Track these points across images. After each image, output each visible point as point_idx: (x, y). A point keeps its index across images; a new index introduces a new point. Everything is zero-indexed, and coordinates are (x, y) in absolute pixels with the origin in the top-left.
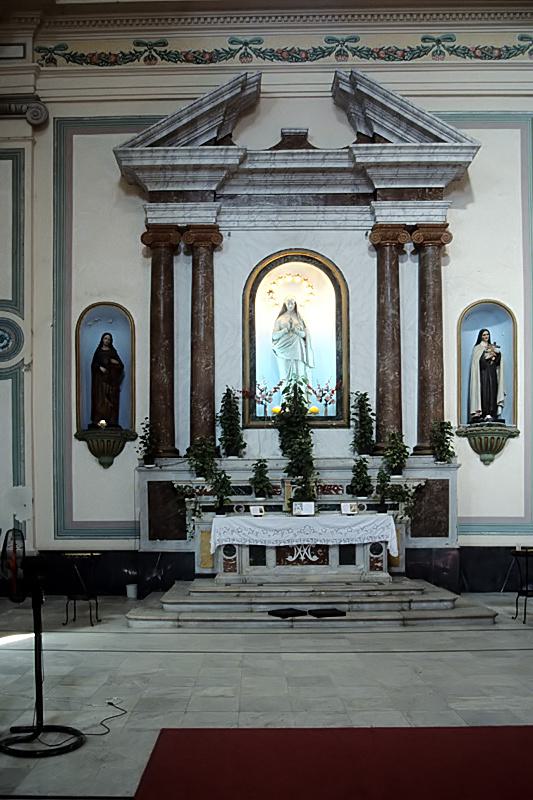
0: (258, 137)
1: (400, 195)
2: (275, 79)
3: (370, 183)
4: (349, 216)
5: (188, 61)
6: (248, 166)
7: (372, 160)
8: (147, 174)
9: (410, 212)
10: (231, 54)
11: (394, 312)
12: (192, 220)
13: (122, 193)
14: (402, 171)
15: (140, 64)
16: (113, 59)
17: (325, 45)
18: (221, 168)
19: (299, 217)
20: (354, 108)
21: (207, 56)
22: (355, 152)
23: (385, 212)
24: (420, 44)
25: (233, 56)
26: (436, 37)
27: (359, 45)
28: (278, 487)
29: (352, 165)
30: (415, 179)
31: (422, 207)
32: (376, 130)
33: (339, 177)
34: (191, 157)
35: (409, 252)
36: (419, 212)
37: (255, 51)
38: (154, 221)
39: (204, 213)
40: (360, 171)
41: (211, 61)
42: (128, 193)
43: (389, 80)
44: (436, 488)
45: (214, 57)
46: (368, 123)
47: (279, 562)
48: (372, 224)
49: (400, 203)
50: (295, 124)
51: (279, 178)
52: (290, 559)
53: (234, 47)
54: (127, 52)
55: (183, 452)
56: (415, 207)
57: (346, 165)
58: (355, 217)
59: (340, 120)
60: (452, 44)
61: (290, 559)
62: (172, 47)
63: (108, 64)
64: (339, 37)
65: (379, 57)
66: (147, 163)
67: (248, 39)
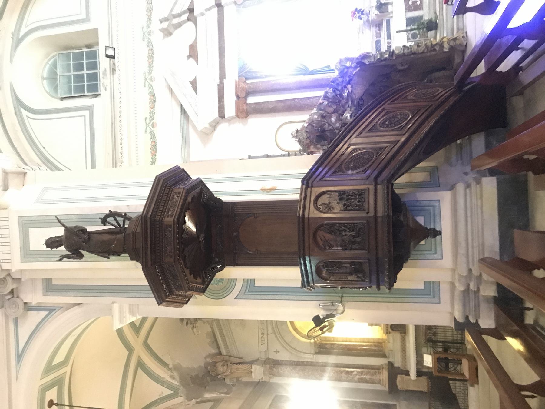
16: (153, 144)
17: (146, 42)
18: (17, 113)
37: (149, 75)
52: (419, 3)
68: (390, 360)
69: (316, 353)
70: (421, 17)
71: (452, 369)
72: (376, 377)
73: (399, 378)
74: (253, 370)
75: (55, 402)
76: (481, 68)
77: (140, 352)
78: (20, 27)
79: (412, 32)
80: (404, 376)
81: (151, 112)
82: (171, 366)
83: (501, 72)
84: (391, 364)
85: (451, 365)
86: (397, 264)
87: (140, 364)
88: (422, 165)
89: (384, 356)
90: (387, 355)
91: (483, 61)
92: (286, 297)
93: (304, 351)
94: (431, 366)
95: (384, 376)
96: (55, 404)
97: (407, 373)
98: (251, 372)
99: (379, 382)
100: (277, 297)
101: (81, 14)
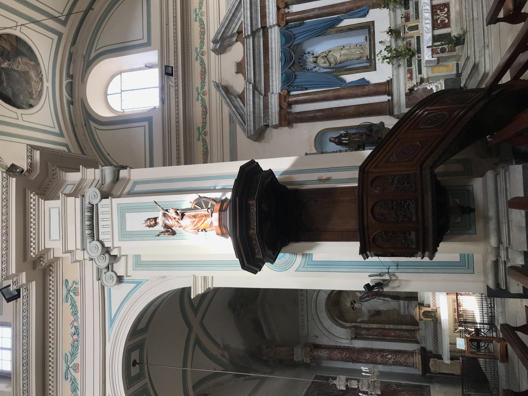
0: (239, 84)
1: (264, 16)
2: (214, 76)
3: (258, 30)
4: (273, 37)
5: (206, 118)
6: (253, 81)
7: (249, 28)
8: (257, 125)
9: (271, 11)
10: (203, 100)
11: (317, 10)
12: (276, 104)
13: (263, 140)
14: (254, 16)
15: (207, 138)
16: (205, 150)
17: (199, 61)
18: (254, 93)
19: (274, 59)
20: (226, 42)
21: (204, 109)
22: (246, 35)
23: (271, 21)
24: (198, 22)
25: (203, 99)
26: (195, 16)
27: (200, 86)
28: (407, 43)
29: (251, 37)
30: (257, 10)
31: (269, 6)
32: (235, 31)
33: (256, 44)
34: (249, 104)
35: (288, 10)
36: (271, 7)
37: (201, 90)
38: (277, 121)
39: (273, 100)
40: (254, 33)
41: (206, 108)
42: (263, 138)
43: (213, 29)
44: (375, 129)
45: (204, 107)
46: (232, 36)
47: (448, 25)
48: (276, 27)
49: (267, 15)
50: (234, 69)
51: (257, 69)
52: (447, 21)
53: (201, 139)
54: (202, 144)
55: (390, 98)
56: (269, 8)
57: (251, 40)
58: (273, 35)
59: (230, 51)
60: (198, 9)
61: (447, 21)
62: (200, 125)
63: (207, 152)
64: (196, 56)
65: (204, 38)
66: (252, 123)
67: (196, 93)
68: (423, 345)
69: (352, 339)
70: (449, 34)
71: (483, 348)
72: (411, 360)
73: (432, 362)
74: (295, 352)
75: (138, 362)
76: (506, 78)
77: (197, 329)
78: (91, 51)
79: (440, 47)
80: (436, 359)
81: (203, 123)
82: (222, 346)
83: (524, 80)
84: (423, 349)
85: (482, 344)
86: (439, 237)
87: (198, 342)
88: (455, 157)
89: (417, 342)
90: (419, 341)
91: (509, 71)
92: (340, 270)
93: (341, 337)
94: (464, 349)
95: (418, 359)
96: (138, 364)
97: (440, 357)
98: (293, 354)
99: (413, 366)
100: (332, 270)
101: (143, 39)
